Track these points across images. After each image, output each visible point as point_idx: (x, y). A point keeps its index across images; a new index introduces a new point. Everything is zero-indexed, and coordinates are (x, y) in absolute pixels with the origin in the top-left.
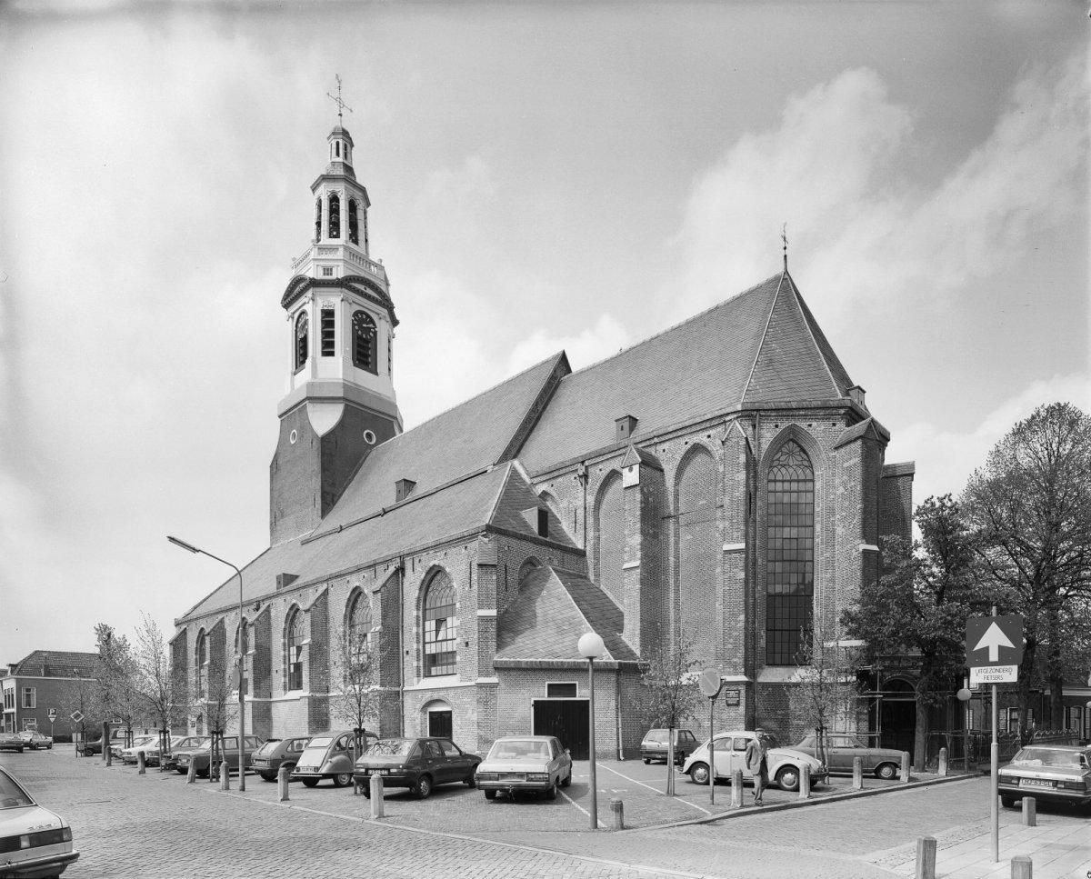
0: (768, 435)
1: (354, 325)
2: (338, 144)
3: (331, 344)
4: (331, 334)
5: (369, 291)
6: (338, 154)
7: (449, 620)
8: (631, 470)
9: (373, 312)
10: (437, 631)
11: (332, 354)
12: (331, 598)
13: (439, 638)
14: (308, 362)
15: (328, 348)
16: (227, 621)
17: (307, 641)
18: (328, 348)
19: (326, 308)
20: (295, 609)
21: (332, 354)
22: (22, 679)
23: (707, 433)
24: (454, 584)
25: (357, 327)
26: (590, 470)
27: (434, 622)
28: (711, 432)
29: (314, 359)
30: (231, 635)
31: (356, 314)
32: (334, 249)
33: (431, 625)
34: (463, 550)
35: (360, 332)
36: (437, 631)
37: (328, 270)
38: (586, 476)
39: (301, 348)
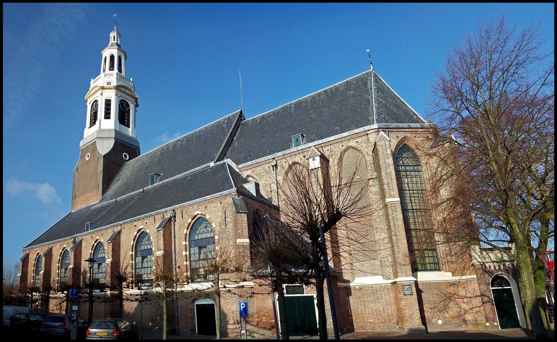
0: (394, 141)
1: (120, 105)
2: (114, 37)
3: (109, 114)
4: (110, 109)
5: (127, 91)
6: (114, 40)
7: (149, 257)
8: (314, 160)
9: (127, 99)
10: (99, 268)
11: (109, 118)
12: (123, 237)
13: (99, 272)
14: (98, 122)
15: (107, 116)
16: (54, 249)
17: (71, 266)
18: (107, 116)
19: (107, 98)
20: (97, 242)
21: (109, 118)
22: (294, 146)
23: (356, 141)
24: (214, 225)
25: (121, 106)
26: (278, 161)
27: (97, 264)
28: (359, 140)
29: (100, 120)
30: (56, 257)
31: (121, 101)
32: (111, 75)
33: (139, 259)
34: (219, 204)
35: (122, 109)
36: (99, 268)
37: (109, 83)
38: (276, 165)
39: (93, 119)
